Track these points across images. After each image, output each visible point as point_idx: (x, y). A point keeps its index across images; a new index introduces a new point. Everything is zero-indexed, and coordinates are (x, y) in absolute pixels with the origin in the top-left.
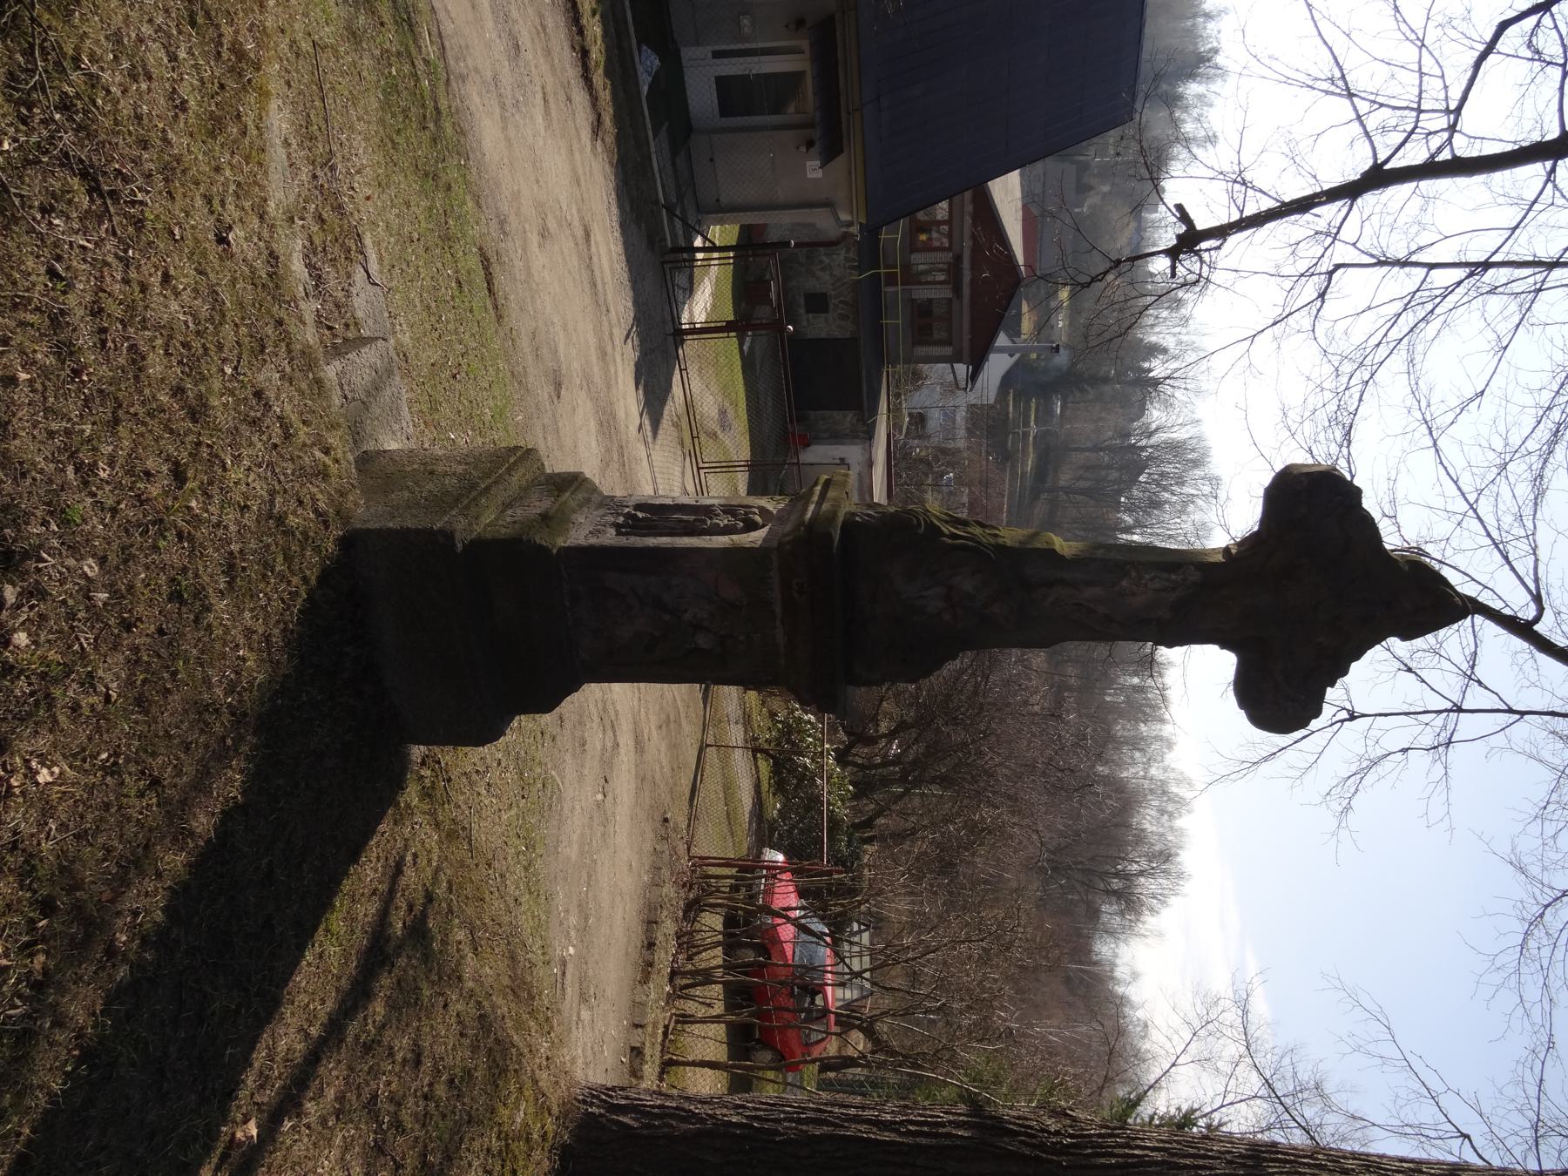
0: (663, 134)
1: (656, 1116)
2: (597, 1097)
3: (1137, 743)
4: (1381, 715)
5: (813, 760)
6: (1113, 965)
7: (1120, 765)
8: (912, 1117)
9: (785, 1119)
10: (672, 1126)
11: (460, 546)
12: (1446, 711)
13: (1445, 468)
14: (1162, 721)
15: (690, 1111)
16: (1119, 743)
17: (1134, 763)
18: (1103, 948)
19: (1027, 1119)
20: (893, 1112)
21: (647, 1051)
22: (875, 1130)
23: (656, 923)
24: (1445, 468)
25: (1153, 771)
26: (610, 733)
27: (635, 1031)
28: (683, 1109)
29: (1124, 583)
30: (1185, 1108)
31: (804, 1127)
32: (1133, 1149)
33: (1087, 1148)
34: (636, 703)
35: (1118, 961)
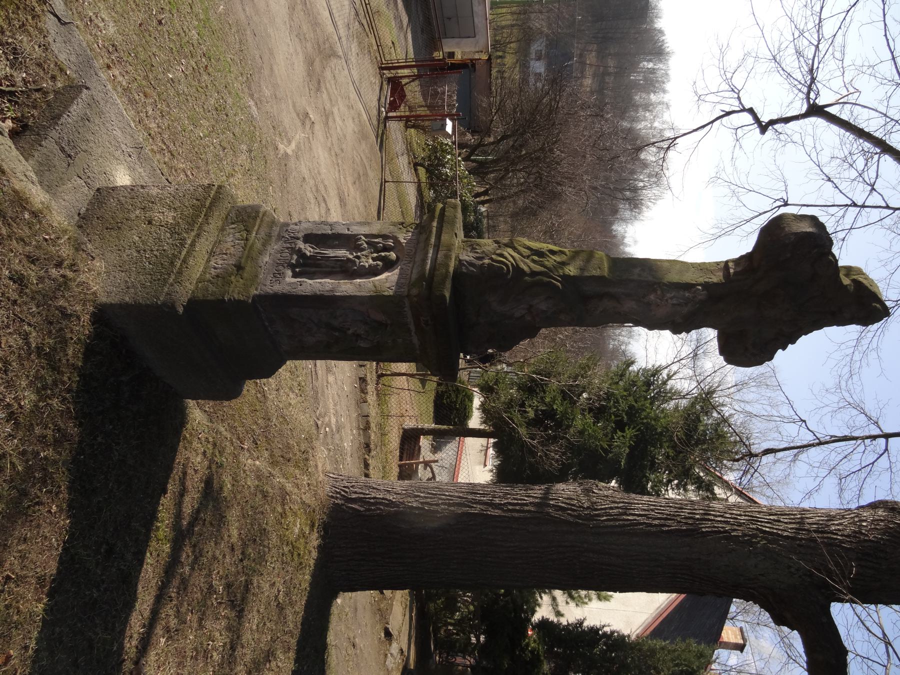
1: (373, 504)
2: (339, 493)
3: (648, 107)
4: (804, 205)
5: (451, 169)
6: (624, 237)
7: (635, 120)
8: (510, 501)
9: (442, 504)
10: (380, 509)
11: (181, 310)
12: (847, 205)
13: (888, 40)
14: (664, 91)
15: (390, 500)
16: (636, 107)
17: (645, 119)
18: (619, 228)
19: (572, 499)
20: (500, 497)
21: (368, 378)
22: (490, 509)
24: (888, 40)
25: (656, 124)
26: (323, 205)
28: (386, 499)
29: (652, 297)
30: (657, 364)
31: (452, 508)
32: (628, 515)
33: (603, 516)
34: (337, 175)
35: (626, 235)
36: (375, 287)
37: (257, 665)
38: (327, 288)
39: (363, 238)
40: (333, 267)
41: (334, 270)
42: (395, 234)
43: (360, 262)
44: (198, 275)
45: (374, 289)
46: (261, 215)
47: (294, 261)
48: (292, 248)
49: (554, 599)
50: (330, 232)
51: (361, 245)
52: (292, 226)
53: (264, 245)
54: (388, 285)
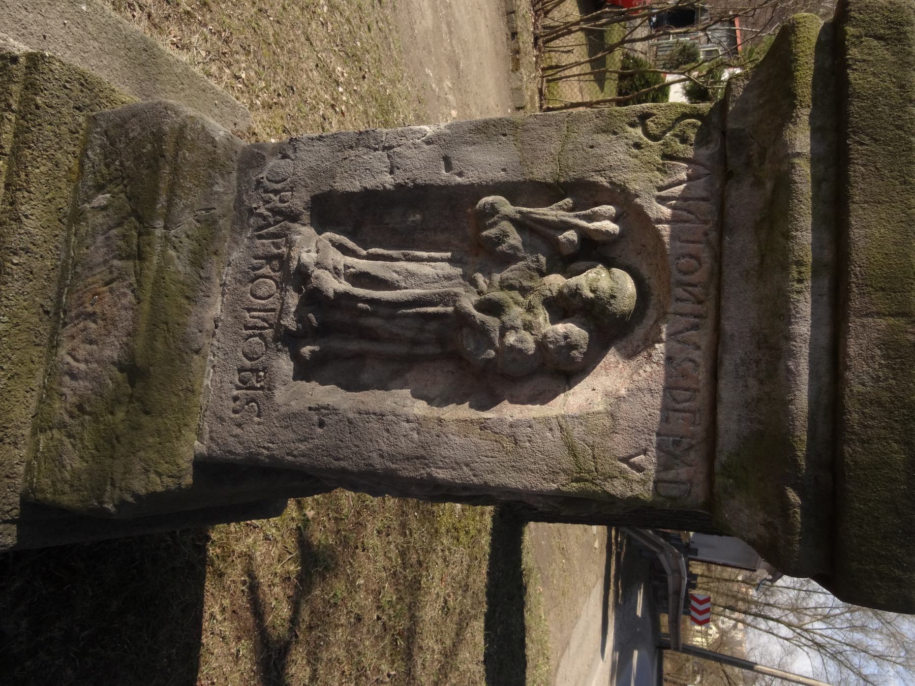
0: (518, 216)
23: (514, 12)
27: (518, 113)
36: (572, 450)
37: (444, 671)
38: (405, 446)
39: (507, 207)
40: (415, 343)
41: (419, 351)
42: (619, 177)
43: (504, 330)
44: (33, 403)
45: (567, 462)
46: (168, 147)
47: (290, 322)
48: (279, 257)
49: (701, 243)
50: (388, 180)
51: (502, 237)
52: (273, 162)
53: (197, 261)
54: (620, 444)
